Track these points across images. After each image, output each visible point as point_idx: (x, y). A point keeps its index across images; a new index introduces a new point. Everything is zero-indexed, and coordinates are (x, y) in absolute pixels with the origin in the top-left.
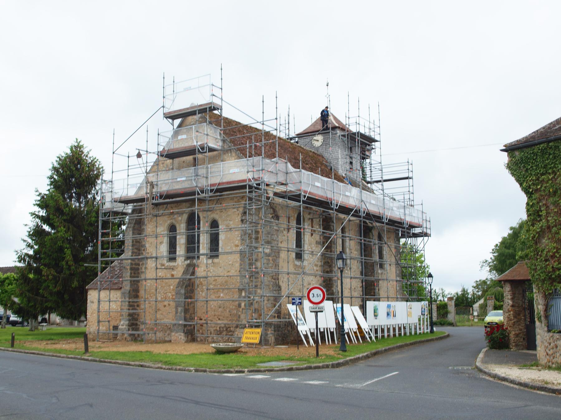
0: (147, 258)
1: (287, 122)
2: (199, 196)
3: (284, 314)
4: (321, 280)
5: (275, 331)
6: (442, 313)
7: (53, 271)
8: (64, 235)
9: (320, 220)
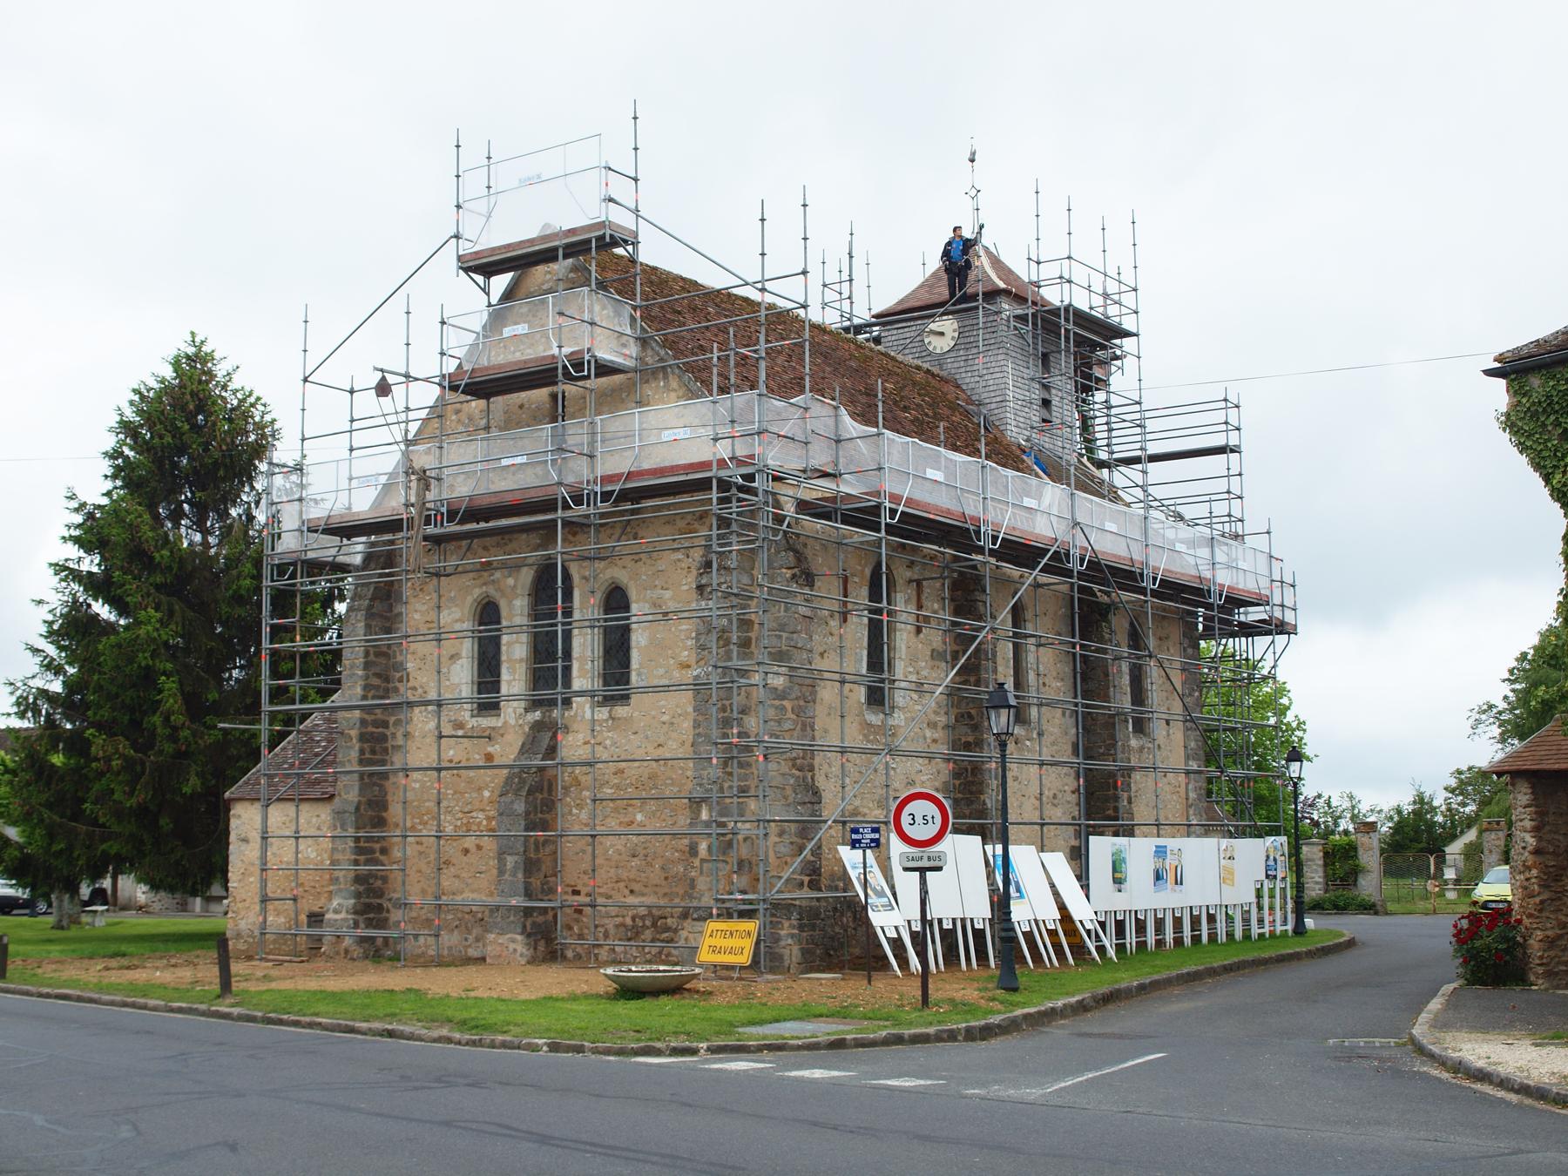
0: (411, 705)
1: (845, 277)
2: (569, 513)
3: (832, 876)
4: (946, 769)
5: (801, 928)
6: (1340, 873)
7: (124, 746)
8: (155, 634)
9: (944, 584)
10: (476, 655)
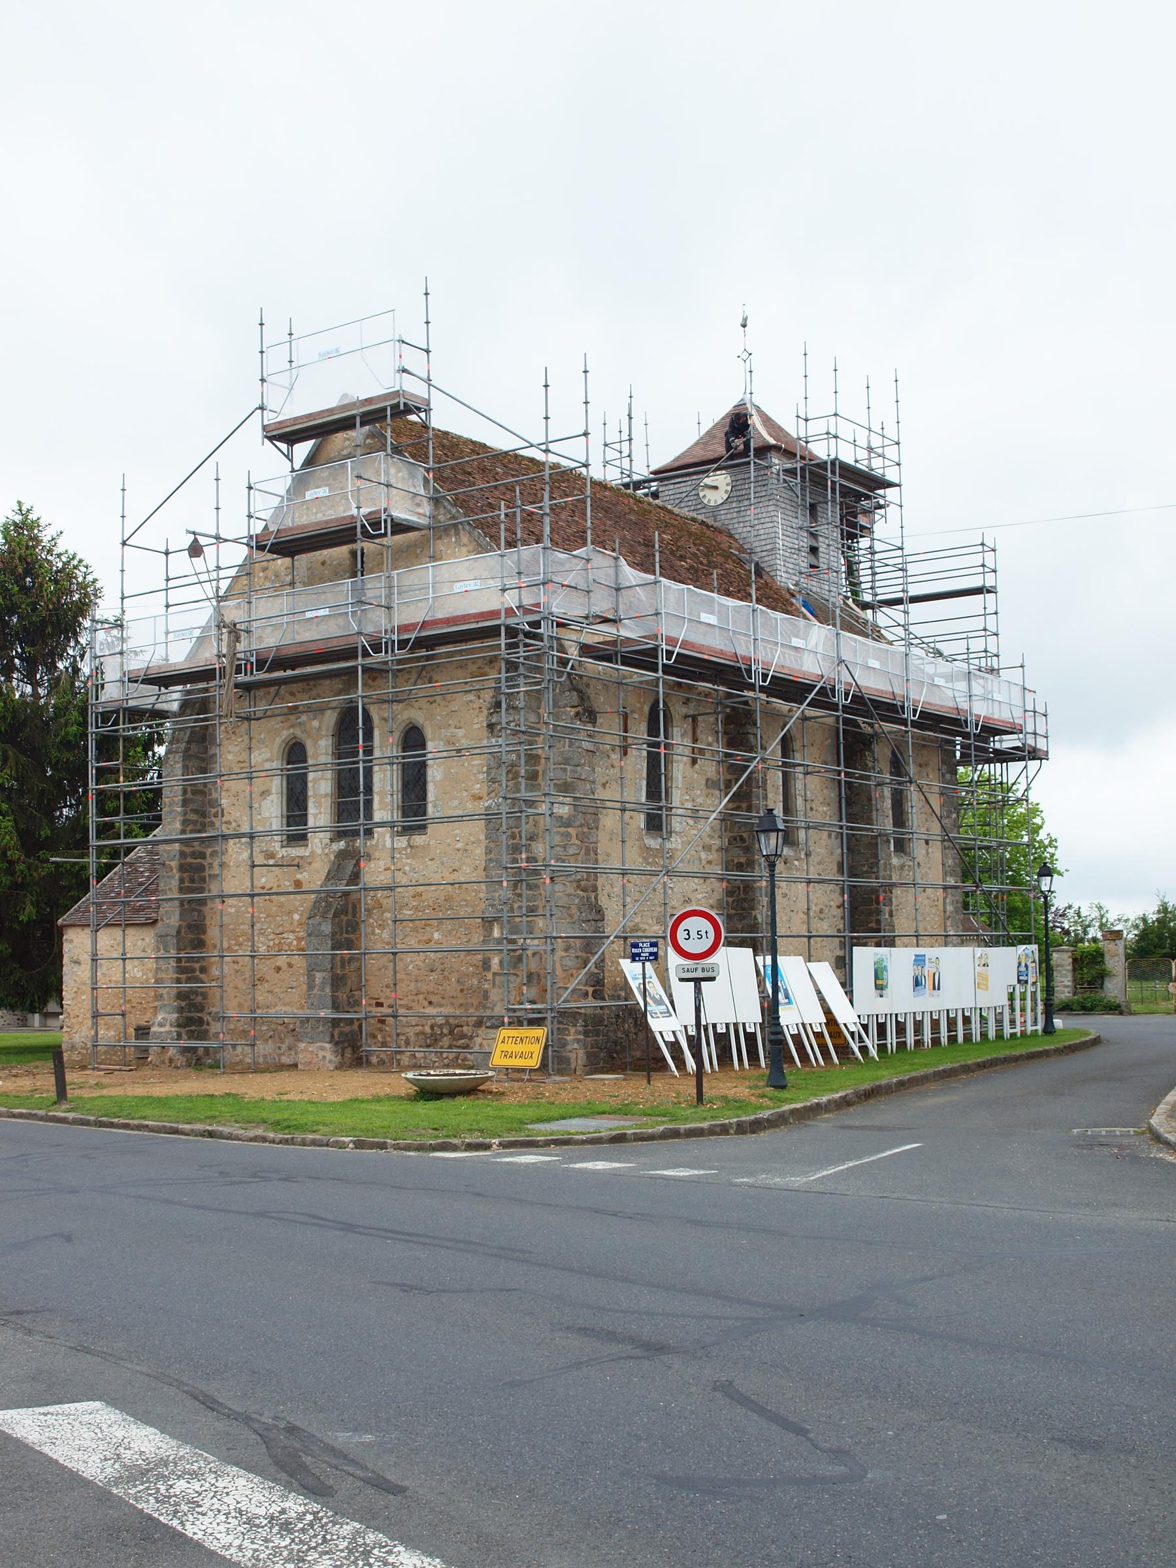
0: (225, 837)
2: (368, 661)
3: (615, 986)
4: (719, 888)
6: (1088, 977)
9: (717, 719)
10: (285, 791)
